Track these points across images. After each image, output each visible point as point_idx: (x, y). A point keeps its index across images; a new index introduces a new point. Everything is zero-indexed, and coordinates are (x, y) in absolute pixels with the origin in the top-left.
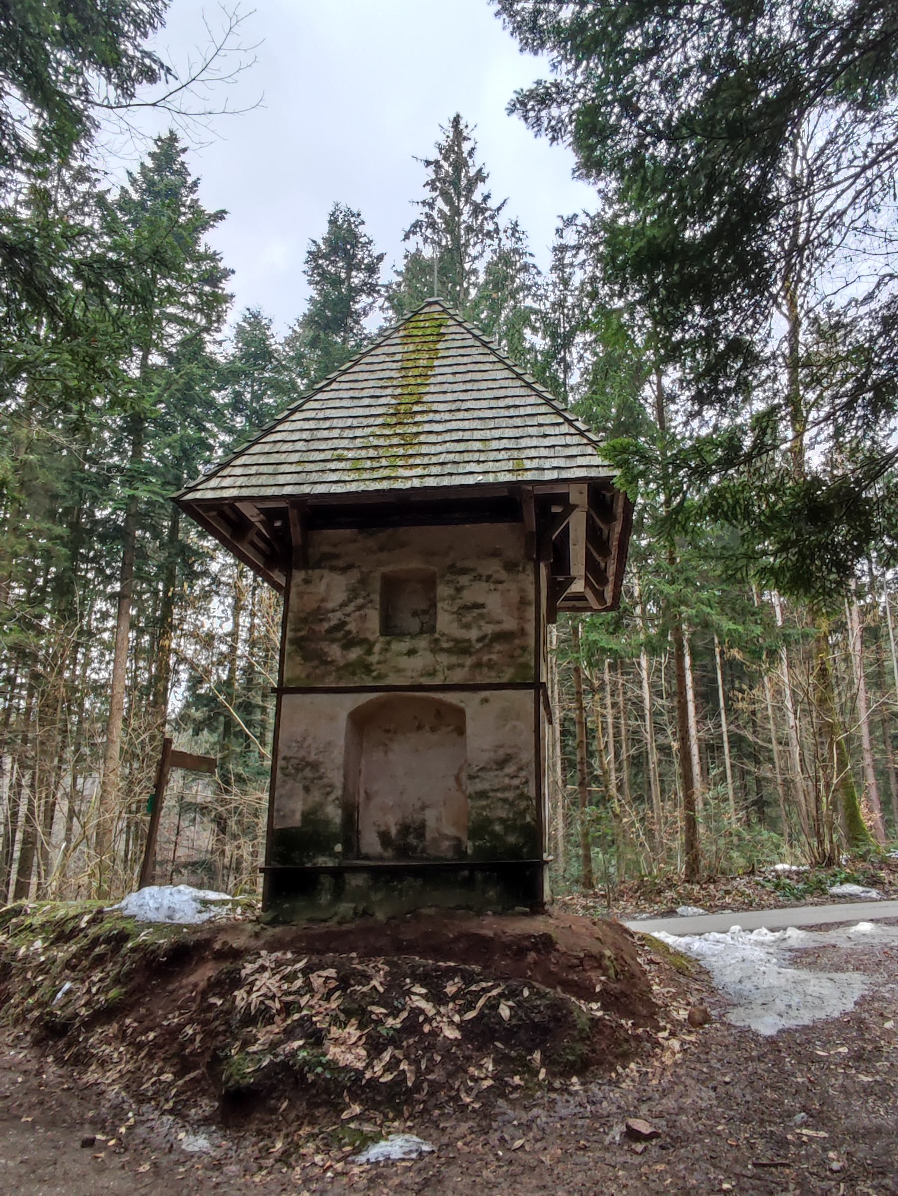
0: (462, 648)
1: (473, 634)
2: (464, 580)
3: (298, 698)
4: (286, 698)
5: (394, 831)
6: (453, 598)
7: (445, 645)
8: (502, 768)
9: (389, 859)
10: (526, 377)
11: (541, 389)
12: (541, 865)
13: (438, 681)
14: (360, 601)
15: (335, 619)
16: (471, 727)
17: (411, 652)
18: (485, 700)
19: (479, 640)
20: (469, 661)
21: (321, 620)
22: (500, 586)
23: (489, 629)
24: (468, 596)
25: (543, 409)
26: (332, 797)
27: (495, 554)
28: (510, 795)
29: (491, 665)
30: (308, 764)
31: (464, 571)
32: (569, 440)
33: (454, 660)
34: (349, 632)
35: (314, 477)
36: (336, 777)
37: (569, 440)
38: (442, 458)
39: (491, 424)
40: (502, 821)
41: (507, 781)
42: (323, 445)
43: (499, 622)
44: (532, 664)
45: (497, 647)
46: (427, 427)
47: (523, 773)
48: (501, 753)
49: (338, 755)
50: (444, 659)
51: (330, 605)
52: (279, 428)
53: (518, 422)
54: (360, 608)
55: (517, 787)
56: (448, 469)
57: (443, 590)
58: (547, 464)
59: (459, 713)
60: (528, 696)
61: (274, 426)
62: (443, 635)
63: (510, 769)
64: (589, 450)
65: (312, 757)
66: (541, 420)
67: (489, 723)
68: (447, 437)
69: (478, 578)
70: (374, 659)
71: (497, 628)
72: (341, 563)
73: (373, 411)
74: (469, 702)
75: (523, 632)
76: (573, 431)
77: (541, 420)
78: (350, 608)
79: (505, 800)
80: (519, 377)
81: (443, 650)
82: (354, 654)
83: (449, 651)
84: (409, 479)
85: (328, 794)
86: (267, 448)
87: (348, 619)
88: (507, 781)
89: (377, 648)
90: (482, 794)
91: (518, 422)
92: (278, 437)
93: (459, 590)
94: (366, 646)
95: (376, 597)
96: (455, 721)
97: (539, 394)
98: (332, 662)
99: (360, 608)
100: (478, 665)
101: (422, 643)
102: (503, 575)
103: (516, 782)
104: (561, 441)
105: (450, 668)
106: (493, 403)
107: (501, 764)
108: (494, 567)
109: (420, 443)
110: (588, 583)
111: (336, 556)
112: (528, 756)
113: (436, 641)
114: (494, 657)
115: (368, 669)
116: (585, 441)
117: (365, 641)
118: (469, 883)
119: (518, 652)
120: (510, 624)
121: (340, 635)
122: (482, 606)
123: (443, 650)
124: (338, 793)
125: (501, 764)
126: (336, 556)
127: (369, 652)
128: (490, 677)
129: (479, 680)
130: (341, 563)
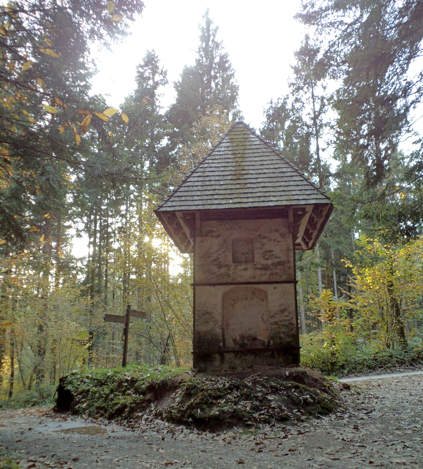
0: (265, 268)
1: (270, 262)
2: (265, 241)
3: (201, 287)
4: (197, 288)
5: (238, 338)
6: (261, 248)
7: (258, 266)
8: (283, 313)
9: (237, 348)
10: (285, 159)
11: (293, 165)
12: (298, 348)
13: (257, 280)
14: (224, 249)
15: (214, 256)
16: (270, 298)
17: (246, 269)
18: (275, 288)
19: (272, 264)
20: (268, 272)
21: (209, 257)
22: (279, 243)
23: (276, 260)
24: (267, 247)
25: (295, 174)
26: (217, 325)
27: (277, 231)
28: (286, 323)
29: (277, 274)
30: (207, 313)
31: (264, 238)
32: (307, 188)
33: (263, 272)
34: (220, 262)
35: (210, 202)
36: (219, 318)
37: (307, 188)
38: (259, 194)
39: (275, 180)
40: (284, 333)
41: (285, 318)
42: (209, 188)
43: (279, 258)
44: (293, 273)
45: (279, 267)
46: (249, 181)
47: (291, 315)
48: (282, 307)
49: (219, 309)
50: (258, 272)
51: (212, 251)
52: (189, 180)
53: (286, 179)
54: (224, 252)
55: (289, 320)
56: (262, 199)
57: (257, 245)
58: (301, 197)
59: (265, 293)
60: (292, 285)
61: (186, 180)
62: (257, 262)
63: (286, 313)
64: (315, 192)
65: (209, 311)
66: (295, 178)
67: (276, 295)
68: (259, 185)
69: (271, 240)
70: (231, 272)
71: (278, 260)
72: (215, 234)
73: (226, 173)
74: (269, 288)
75: (289, 262)
76: (308, 184)
77: (295, 178)
78: (220, 252)
79: (284, 325)
80: (282, 159)
81: (258, 268)
82: (223, 270)
83: (261, 269)
84: (249, 203)
85: (216, 324)
86: (186, 189)
87: (220, 257)
88: (285, 318)
89: (232, 268)
90: (276, 323)
91: (286, 179)
92: (189, 184)
93: (263, 245)
94: (228, 267)
95: (230, 248)
96: (264, 296)
97: (292, 167)
98: (215, 273)
99: (224, 252)
100: (272, 274)
101: (249, 266)
102: (280, 239)
103: (289, 318)
104: (304, 188)
105: (261, 275)
106: (274, 171)
107: (283, 311)
108: (276, 236)
109: (248, 188)
110: (303, 239)
111: (212, 231)
112: (293, 308)
113: (255, 265)
114: (278, 271)
115: (229, 276)
116: (313, 188)
117: (227, 265)
118: (272, 355)
119: (287, 269)
120: (283, 258)
121: (217, 263)
122: (272, 251)
123: (258, 268)
124: (220, 323)
125: (283, 311)
126: (212, 231)
127: (229, 269)
128: (277, 279)
129: (273, 280)
130: (215, 234)
